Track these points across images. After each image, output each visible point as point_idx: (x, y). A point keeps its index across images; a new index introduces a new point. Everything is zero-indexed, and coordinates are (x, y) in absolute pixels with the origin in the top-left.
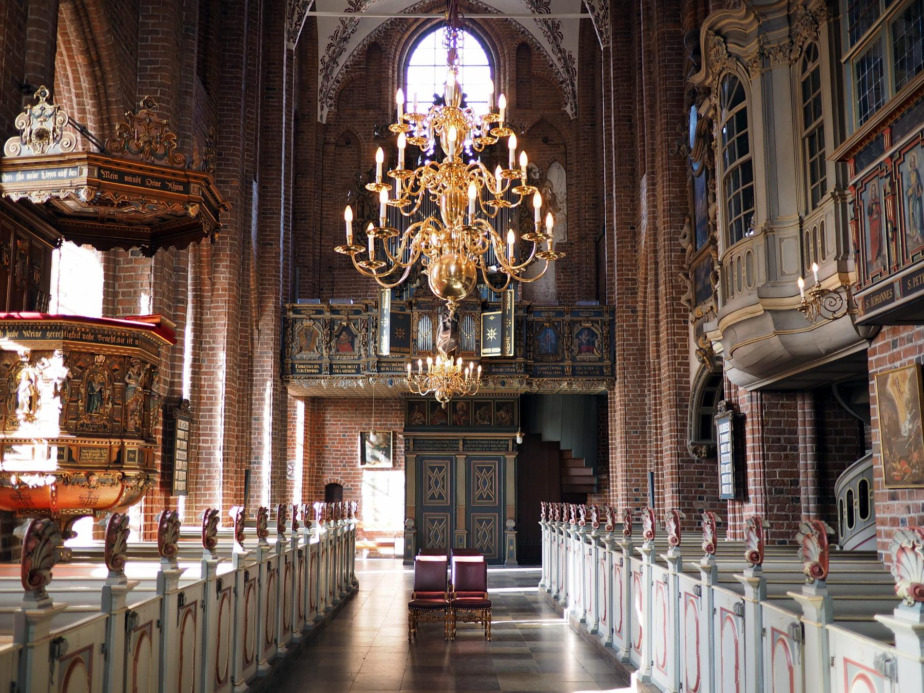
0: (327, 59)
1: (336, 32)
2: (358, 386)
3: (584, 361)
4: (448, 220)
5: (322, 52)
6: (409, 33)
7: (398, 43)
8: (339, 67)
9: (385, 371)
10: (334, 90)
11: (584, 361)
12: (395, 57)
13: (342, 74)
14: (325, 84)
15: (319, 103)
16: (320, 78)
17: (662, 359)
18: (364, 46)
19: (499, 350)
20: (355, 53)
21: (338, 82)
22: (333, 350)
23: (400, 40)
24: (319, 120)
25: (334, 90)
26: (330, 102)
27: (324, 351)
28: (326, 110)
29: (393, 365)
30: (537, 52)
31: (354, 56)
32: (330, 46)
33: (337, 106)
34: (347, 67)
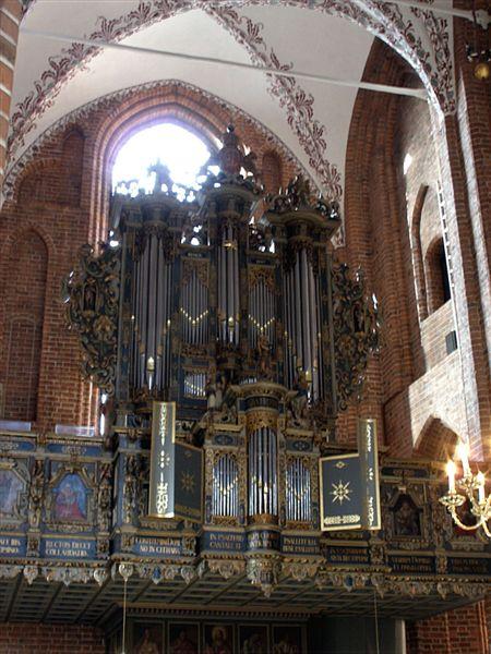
1: (28, 100)
2: (93, 581)
3: (463, 550)
6: (121, 121)
8: (26, 147)
10: (14, 174)
11: (463, 550)
12: (101, 146)
13: (28, 157)
20: (48, 133)
21: (21, 165)
22: (48, 514)
25: (14, 174)
27: (31, 516)
30: (289, 164)
31: (46, 137)
33: (18, 197)
34: (35, 149)
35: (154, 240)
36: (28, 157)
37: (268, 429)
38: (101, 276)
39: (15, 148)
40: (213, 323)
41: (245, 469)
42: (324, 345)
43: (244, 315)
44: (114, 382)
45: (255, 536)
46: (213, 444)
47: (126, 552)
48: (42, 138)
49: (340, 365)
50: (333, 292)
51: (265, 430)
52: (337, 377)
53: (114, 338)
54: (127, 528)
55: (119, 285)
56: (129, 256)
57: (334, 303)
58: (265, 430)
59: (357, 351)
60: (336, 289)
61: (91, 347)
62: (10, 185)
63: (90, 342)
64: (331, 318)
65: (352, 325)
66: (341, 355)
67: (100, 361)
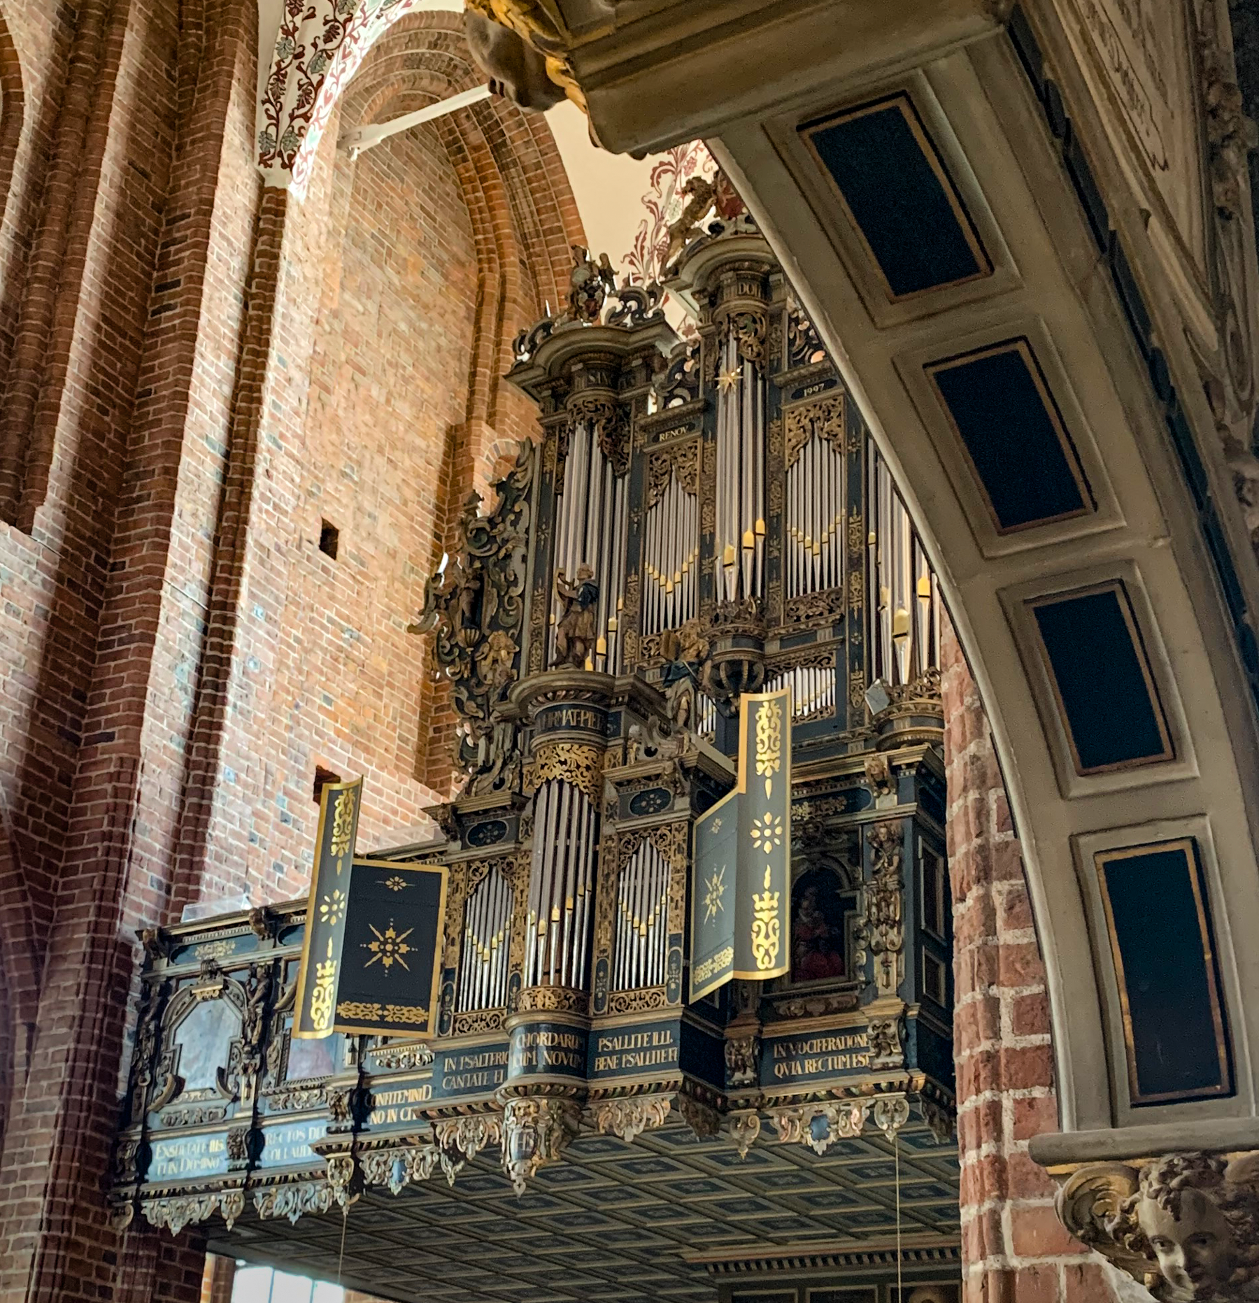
37: (561, 782)
51: (555, 787)
63: (472, 697)
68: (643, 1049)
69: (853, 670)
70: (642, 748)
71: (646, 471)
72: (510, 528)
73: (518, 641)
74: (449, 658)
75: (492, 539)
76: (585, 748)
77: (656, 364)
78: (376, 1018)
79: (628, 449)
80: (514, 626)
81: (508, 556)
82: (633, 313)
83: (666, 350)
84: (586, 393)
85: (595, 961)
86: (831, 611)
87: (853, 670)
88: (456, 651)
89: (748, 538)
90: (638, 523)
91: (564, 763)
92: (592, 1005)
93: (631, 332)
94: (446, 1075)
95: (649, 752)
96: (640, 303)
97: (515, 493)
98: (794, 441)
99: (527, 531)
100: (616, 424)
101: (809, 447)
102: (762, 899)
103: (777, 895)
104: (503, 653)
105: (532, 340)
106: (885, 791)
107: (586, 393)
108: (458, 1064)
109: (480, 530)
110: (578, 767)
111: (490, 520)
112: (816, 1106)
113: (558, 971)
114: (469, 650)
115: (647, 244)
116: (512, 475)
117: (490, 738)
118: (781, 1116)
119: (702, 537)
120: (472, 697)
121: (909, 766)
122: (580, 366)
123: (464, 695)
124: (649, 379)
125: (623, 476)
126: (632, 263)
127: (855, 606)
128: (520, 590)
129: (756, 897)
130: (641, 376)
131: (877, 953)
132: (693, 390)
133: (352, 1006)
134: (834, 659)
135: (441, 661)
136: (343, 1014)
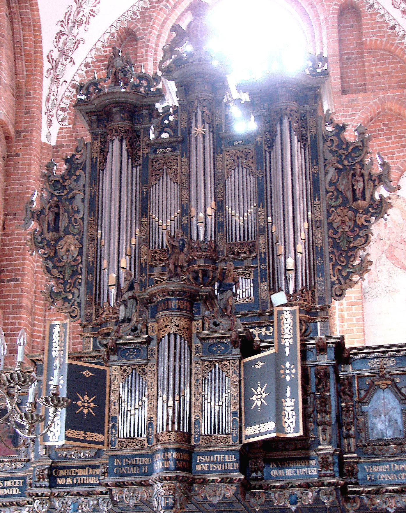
0: (55, 55)
1: (68, 15)
4: (329, 377)
5: (48, 44)
7: (162, 27)
8: (77, 64)
9: (65, 485)
10: (68, 98)
13: (81, 76)
14: (54, 88)
15: (44, 118)
16: (46, 82)
17: (315, 32)
18: (112, 34)
19: (271, 425)
20: (99, 45)
23: (164, 22)
24: (44, 139)
25: (68, 98)
26: (63, 115)
28: (56, 127)
29: (80, 472)
31: (98, 50)
32: (60, 34)
34: (87, 65)
35: (117, 143)
36: (81, 76)
37: (175, 335)
38: (65, 192)
39: (63, 71)
40: (185, 222)
41: (155, 383)
42: (315, 224)
43: (220, 207)
44: (79, 305)
45: (159, 456)
46: (119, 359)
47: (41, 486)
48: (94, 52)
49: (335, 245)
50: (325, 160)
51: (172, 337)
52: (331, 259)
53: (79, 258)
54: (32, 456)
55: (83, 200)
56: (93, 166)
57: (326, 173)
58: (172, 337)
59: (356, 225)
60: (329, 156)
61: (55, 272)
62: (63, 110)
63: (55, 267)
64: (322, 191)
65: (349, 195)
66: (336, 232)
67: (65, 283)
68: (220, 462)
69: (262, 281)
70: (212, 321)
71: (150, 167)
72: (73, 183)
73: (81, 242)
74: (41, 245)
75: (64, 187)
76: (186, 320)
77: (155, 114)
78: (82, 438)
79: (140, 154)
80: (79, 234)
81: (73, 197)
82: (145, 87)
83: (159, 106)
84: (119, 122)
85: (193, 421)
86: (250, 252)
87: (262, 281)
88: (45, 242)
89: (209, 211)
90: (147, 192)
91: (177, 326)
92: (193, 440)
93: (144, 97)
94: (116, 466)
95: (215, 324)
96: (149, 83)
97: (76, 166)
98: (229, 167)
99: (84, 186)
100: (134, 139)
101: (237, 169)
102: (286, 402)
103: (293, 400)
104: (72, 247)
105: (87, 89)
106: (322, 353)
107: (119, 122)
108: (122, 462)
109: (56, 181)
110: (184, 328)
111: (62, 177)
112: (292, 490)
113: (173, 423)
114: (52, 243)
115: (71, 18)
116: (73, 156)
117: (126, 306)
118: (275, 493)
119: (182, 206)
120: (55, 267)
121: (333, 343)
122: (118, 109)
123: (50, 265)
124: (150, 121)
125: (136, 167)
126: (62, 26)
127: (262, 251)
128: (81, 216)
129: (283, 400)
130: (146, 119)
131: (319, 425)
132: (175, 130)
133: (71, 432)
134: (252, 275)
135: (36, 246)
136: (68, 435)
